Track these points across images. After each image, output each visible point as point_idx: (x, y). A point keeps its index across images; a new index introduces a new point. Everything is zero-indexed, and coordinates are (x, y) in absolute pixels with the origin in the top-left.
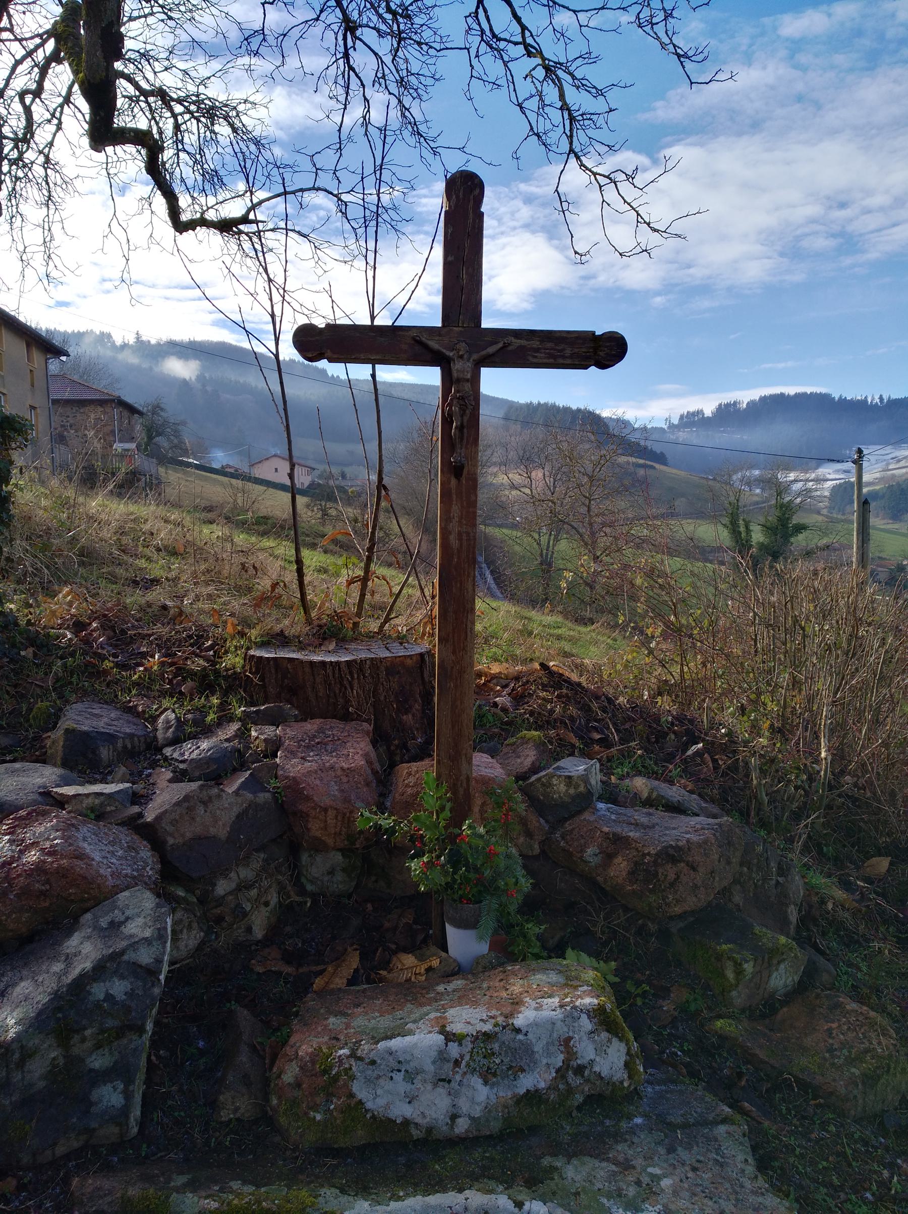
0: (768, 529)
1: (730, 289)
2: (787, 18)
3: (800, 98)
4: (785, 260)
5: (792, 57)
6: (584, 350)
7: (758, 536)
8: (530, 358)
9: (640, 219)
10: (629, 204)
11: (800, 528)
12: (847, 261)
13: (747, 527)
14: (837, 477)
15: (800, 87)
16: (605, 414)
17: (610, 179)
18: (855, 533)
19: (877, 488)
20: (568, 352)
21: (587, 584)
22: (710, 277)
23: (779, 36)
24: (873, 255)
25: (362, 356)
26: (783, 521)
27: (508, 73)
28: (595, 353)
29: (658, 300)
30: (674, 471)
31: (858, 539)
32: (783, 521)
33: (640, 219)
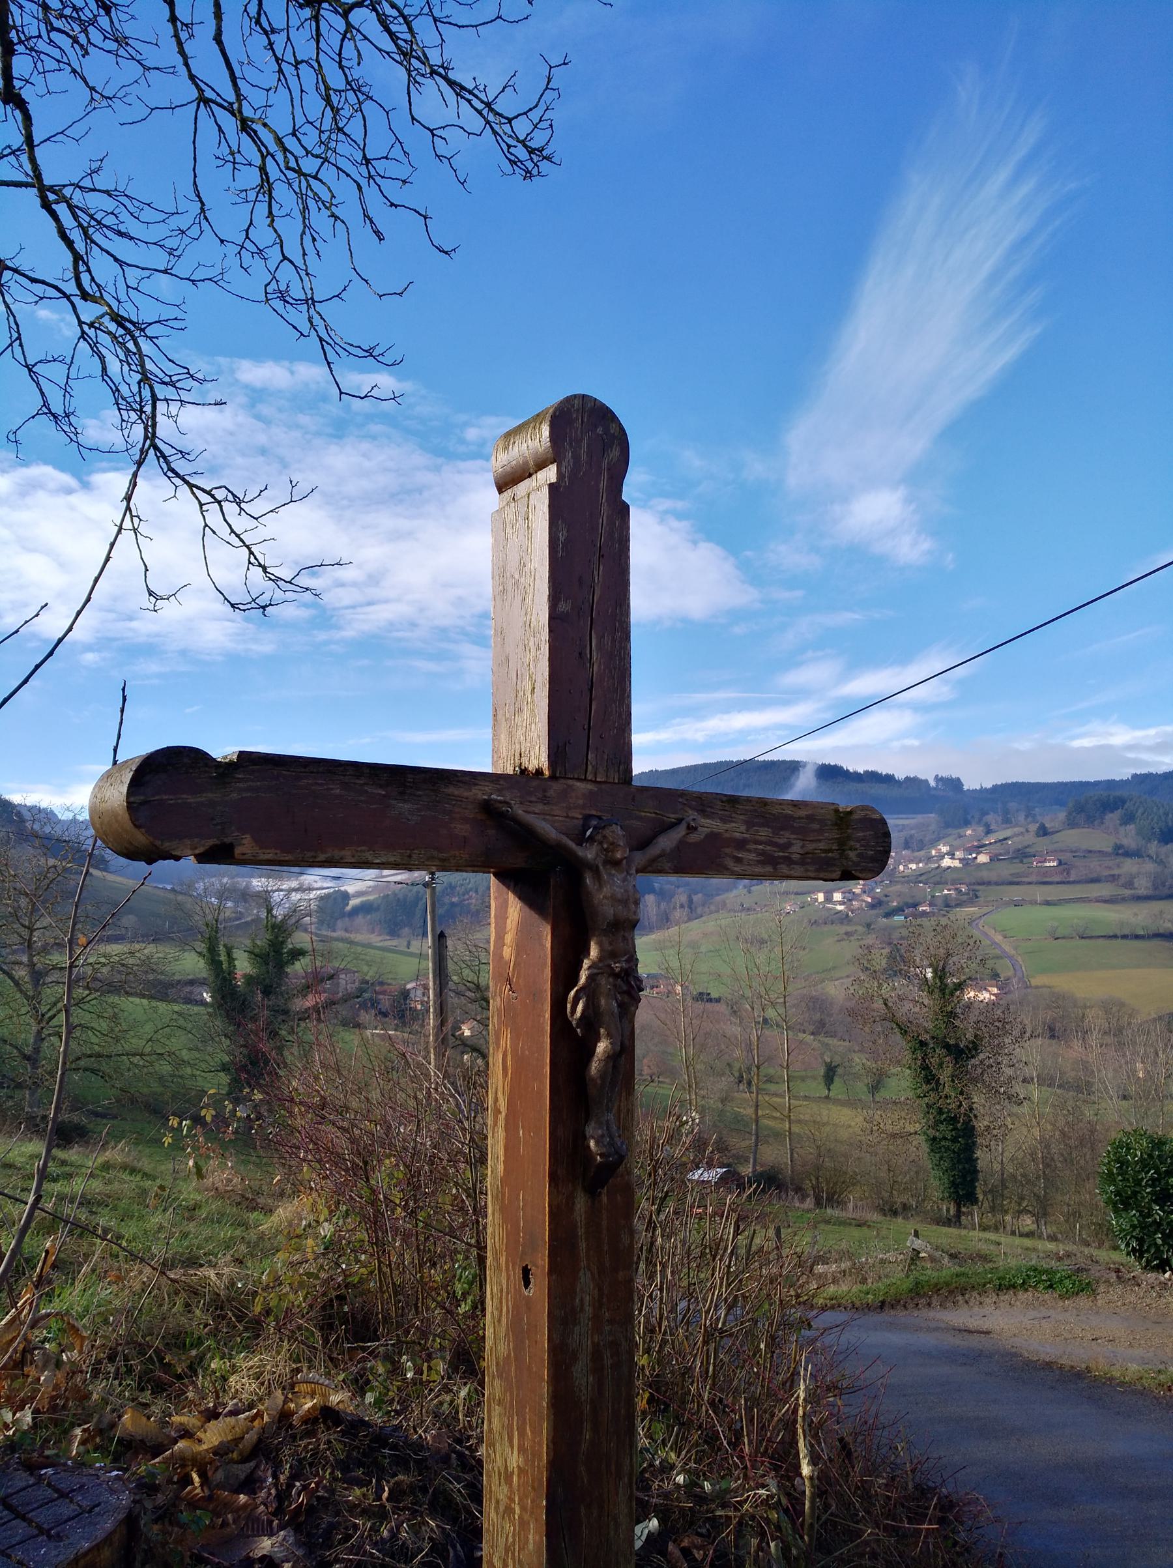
0: (258, 956)
1: (183, 653)
2: (245, 364)
3: (263, 451)
4: (251, 626)
5: (253, 406)
6: (822, 845)
7: (243, 966)
8: (730, 863)
9: (253, 560)
10: (238, 536)
11: (297, 954)
12: (322, 636)
13: (229, 954)
14: (325, 885)
15: (262, 439)
16: (16, 799)
17: (213, 496)
18: (431, 976)
19: (371, 898)
20: (796, 849)
21: (27, 1058)
22: (158, 635)
23: (237, 380)
24: (349, 633)
25: (347, 853)
26: (276, 945)
27: (11, 318)
28: (842, 851)
29: (90, 657)
30: (119, 879)
31: (435, 984)
32: (276, 945)
33: (253, 560)
